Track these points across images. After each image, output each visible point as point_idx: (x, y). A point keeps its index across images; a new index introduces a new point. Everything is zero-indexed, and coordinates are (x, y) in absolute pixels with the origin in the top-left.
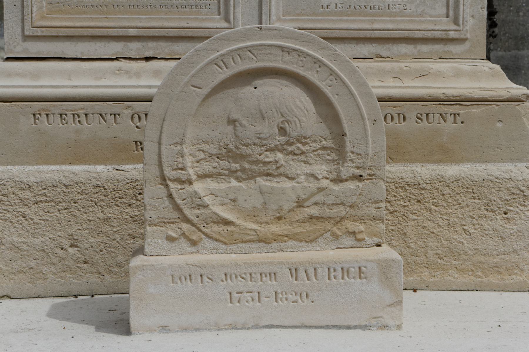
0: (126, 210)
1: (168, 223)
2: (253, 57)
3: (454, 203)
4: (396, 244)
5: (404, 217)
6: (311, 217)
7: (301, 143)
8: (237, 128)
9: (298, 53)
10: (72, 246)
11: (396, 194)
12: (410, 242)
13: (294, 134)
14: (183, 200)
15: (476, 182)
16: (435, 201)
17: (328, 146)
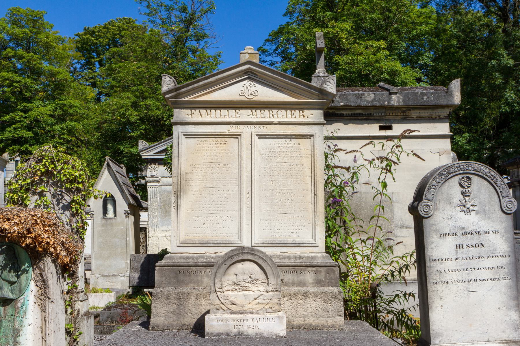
13: (254, 278)
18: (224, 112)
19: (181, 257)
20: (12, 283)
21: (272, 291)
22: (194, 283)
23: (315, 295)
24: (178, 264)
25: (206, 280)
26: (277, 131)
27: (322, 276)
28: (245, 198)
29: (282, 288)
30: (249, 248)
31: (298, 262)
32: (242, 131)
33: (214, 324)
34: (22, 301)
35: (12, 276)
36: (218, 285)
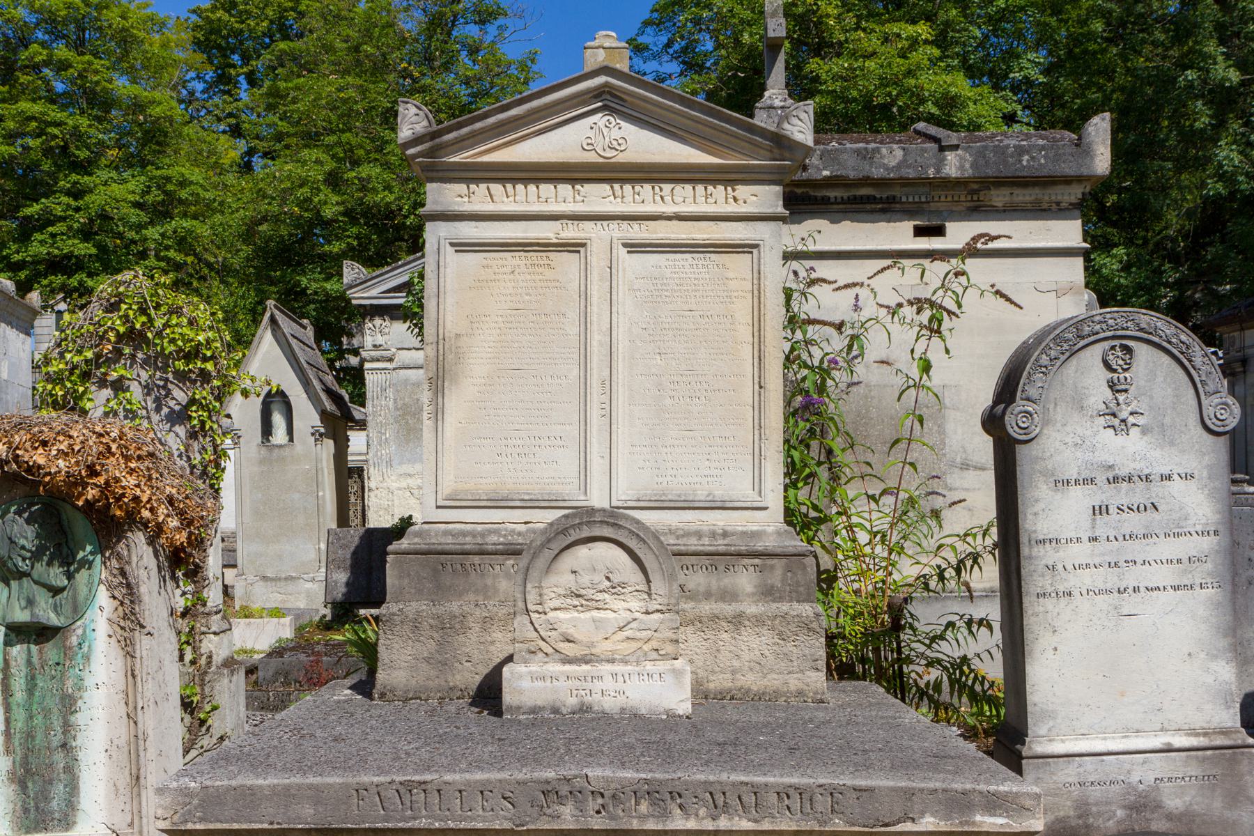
18: (547, 189)
19: (446, 533)
20: (56, 591)
21: (658, 611)
22: (476, 592)
23: (759, 621)
24: (440, 547)
25: (503, 585)
26: (673, 236)
27: (776, 577)
28: (596, 396)
29: (683, 606)
30: (604, 510)
31: (720, 545)
32: (588, 235)
33: (525, 685)
34: (80, 632)
35: (56, 576)
36: (532, 597)
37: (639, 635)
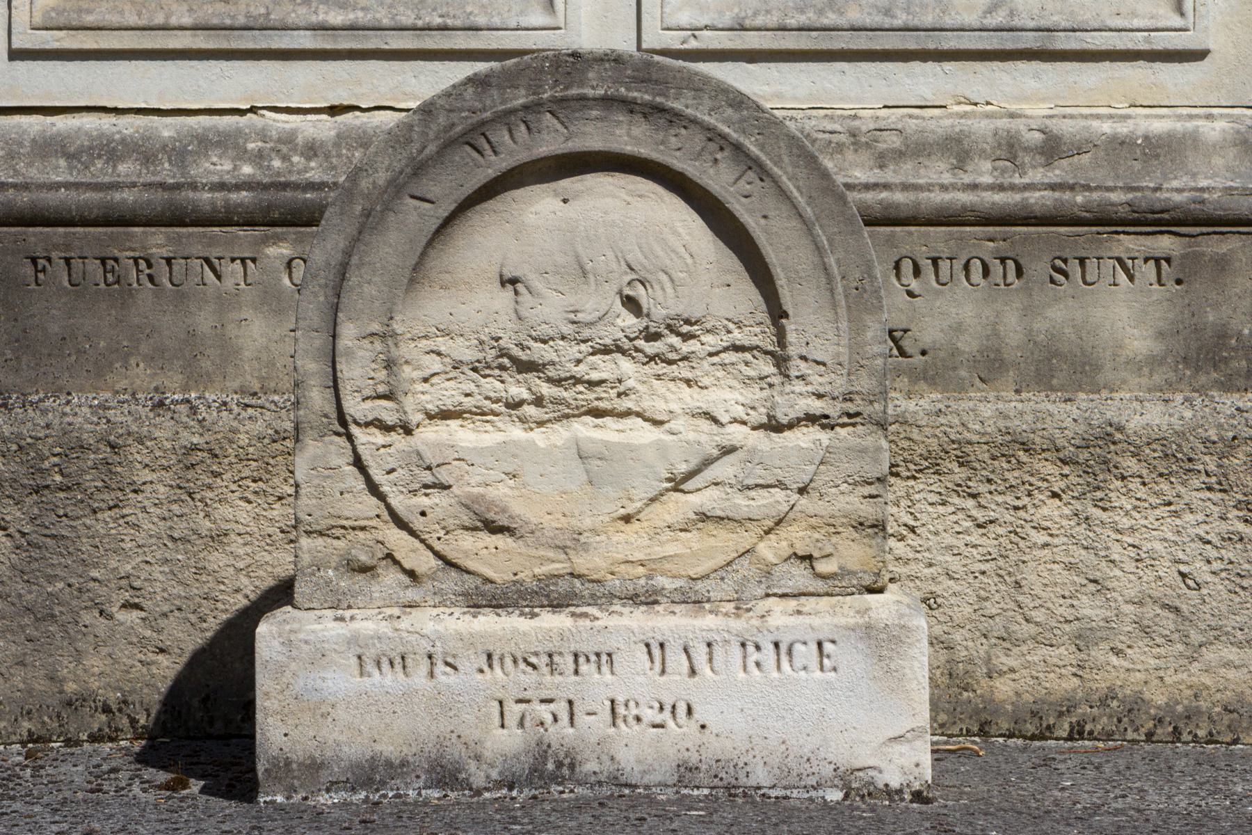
0: (268, 514)
1: (354, 529)
2: (559, 126)
3: (1154, 500)
4: (994, 611)
5: (1016, 539)
6: (704, 517)
7: (679, 334)
8: (520, 299)
9: (667, 116)
10: (127, 606)
11: (992, 476)
12: (1032, 605)
13: (659, 313)
14: (389, 473)
15: (1214, 443)
16: (1099, 494)
17: (747, 343)
19: (47, 147)
21: (811, 419)
22: (158, 358)
23: (1171, 458)
24: (24, 198)
25: (256, 333)
29: (900, 404)
30: (615, 59)
31: (1036, 186)
33: (333, 684)
36: (358, 371)
37: (741, 504)
